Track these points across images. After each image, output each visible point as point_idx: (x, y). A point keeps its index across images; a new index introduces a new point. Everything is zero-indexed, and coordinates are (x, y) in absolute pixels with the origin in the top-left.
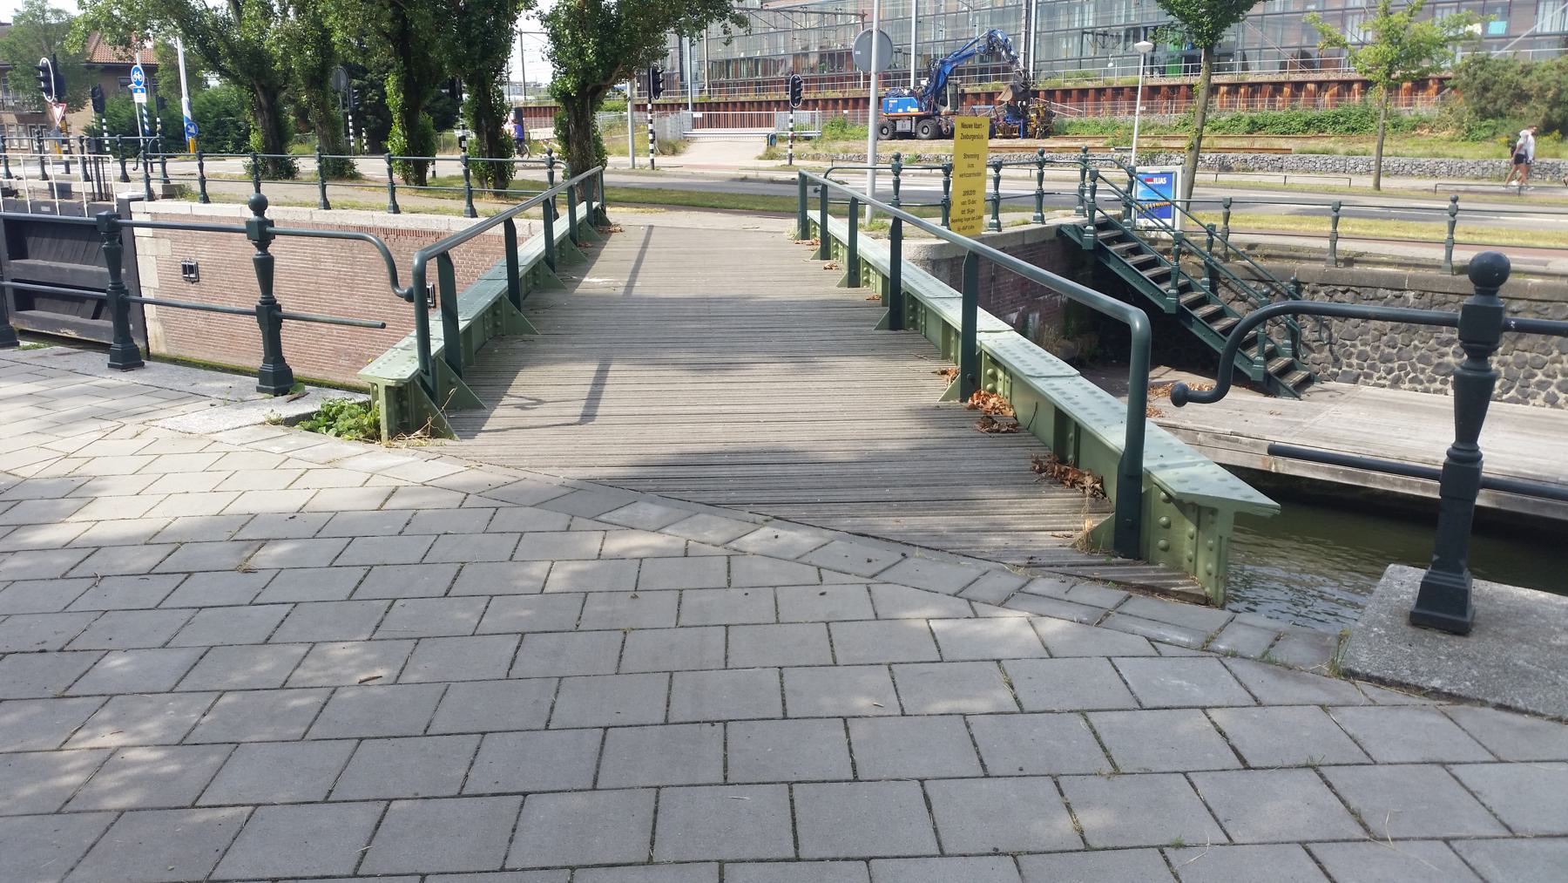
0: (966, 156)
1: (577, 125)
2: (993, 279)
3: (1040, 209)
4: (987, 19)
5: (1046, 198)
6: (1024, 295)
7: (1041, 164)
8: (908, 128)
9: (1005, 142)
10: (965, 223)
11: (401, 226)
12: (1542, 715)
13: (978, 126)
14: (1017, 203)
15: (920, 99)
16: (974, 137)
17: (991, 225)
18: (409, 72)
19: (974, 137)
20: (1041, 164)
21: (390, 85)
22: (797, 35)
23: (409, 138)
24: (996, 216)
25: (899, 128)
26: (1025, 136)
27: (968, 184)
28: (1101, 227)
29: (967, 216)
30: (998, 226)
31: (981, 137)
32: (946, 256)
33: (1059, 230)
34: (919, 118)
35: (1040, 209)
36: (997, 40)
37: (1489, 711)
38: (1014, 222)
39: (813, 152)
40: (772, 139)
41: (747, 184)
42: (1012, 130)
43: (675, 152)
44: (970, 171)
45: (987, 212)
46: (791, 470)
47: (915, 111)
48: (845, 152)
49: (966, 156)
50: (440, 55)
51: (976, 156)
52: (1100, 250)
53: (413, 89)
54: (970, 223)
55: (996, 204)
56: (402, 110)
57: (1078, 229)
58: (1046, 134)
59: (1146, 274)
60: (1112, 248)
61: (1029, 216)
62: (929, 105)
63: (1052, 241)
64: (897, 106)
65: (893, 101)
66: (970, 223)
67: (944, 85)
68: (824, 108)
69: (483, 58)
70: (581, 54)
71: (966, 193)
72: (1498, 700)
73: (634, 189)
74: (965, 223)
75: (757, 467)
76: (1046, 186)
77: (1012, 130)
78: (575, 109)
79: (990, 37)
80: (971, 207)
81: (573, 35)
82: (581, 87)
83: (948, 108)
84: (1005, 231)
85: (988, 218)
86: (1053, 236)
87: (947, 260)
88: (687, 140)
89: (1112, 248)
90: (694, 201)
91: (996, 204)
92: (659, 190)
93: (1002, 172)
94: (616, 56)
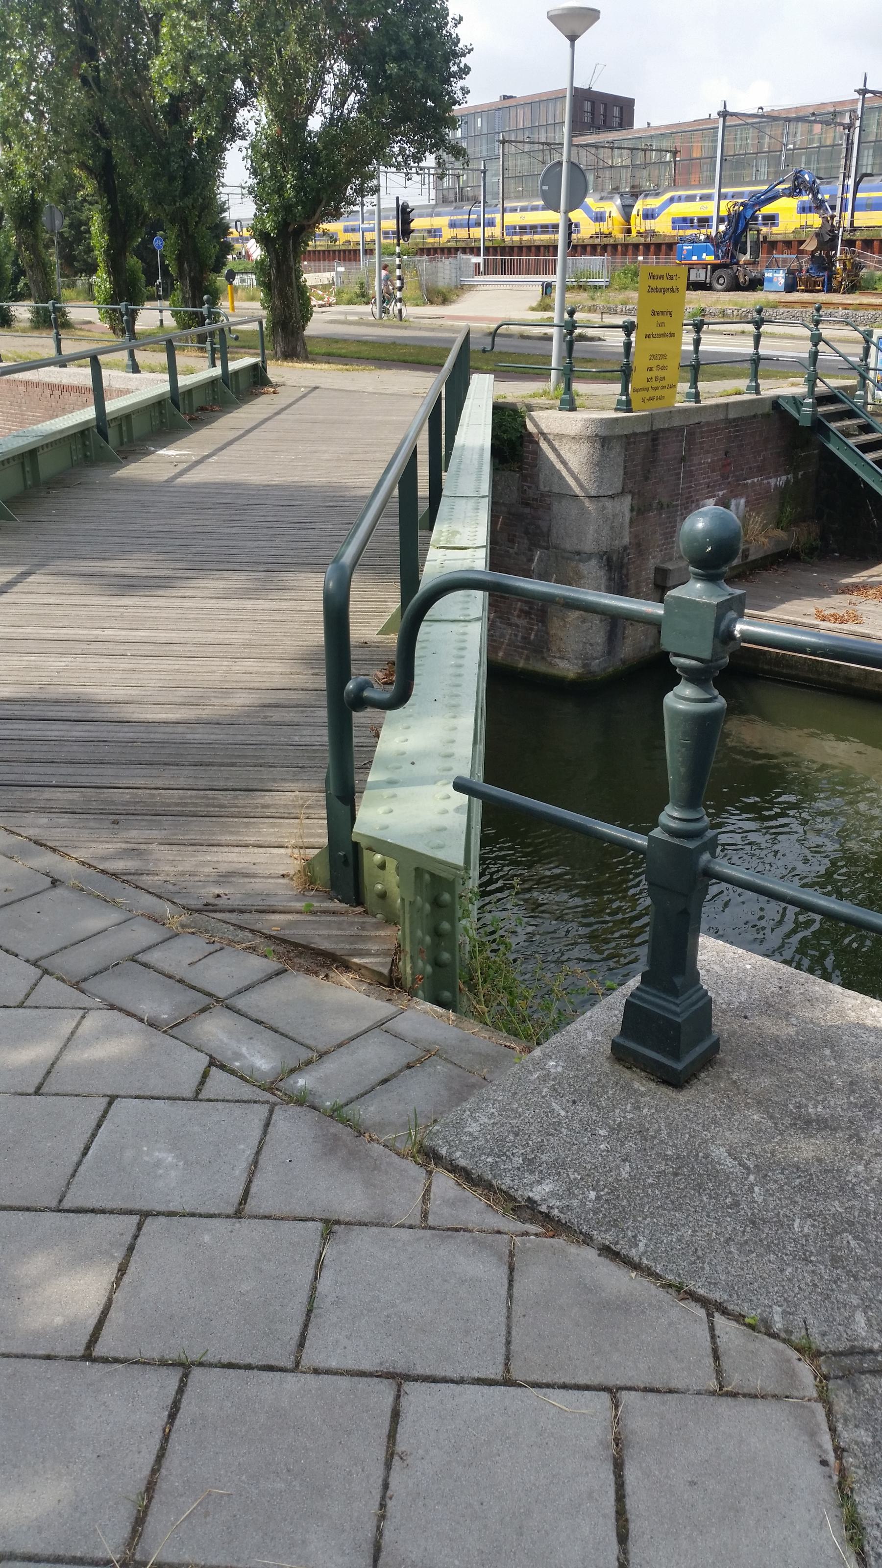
0: (654, 313)
1: (279, 270)
2: (683, 459)
3: (755, 376)
4: (814, 158)
5: (762, 365)
6: (724, 477)
7: (758, 324)
8: (702, 278)
9: (807, 297)
10: (652, 393)
11: (65, 381)
12: (657, 1277)
13: (671, 278)
14: (724, 366)
15: (717, 246)
16: (665, 290)
17: (688, 395)
18: (114, 210)
19: (665, 290)
20: (758, 324)
21: (96, 226)
22: (607, 173)
23: (116, 284)
24: (694, 384)
25: (693, 278)
26: (830, 290)
27: (659, 345)
28: (822, 400)
29: (655, 384)
30: (697, 397)
31: (675, 290)
32: (618, 431)
33: (775, 403)
34: (715, 267)
35: (755, 376)
36: (804, 181)
37: (590, 1254)
38: (718, 392)
39: (590, 303)
40: (547, 288)
41: (528, 343)
42: (816, 283)
43: (445, 300)
44: (661, 330)
45: (683, 380)
46: (55, 731)
47: (710, 258)
48: (625, 303)
49: (654, 313)
50: (139, 192)
51: (669, 313)
52: (819, 426)
53: (119, 227)
54: (659, 393)
55: (696, 369)
56: (107, 252)
57: (796, 401)
58: (853, 288)
59: (869, 457)
60: (833, 426)
61: (743, 384)
62: (727, 253)
63: (766, 416)
64: (691, 253)
65: (687, 247)
66: (659, 393)
67: (745, 230)
68: (614, 254)
69: (185, 193)
70: (280, 190)
71: (653, 357)
72: (607, 1238)
73: (365, 343)
74: (652, 393)
75: (39, 725)
76: (762, 351)
77: (816, 283)
78: (275, 250)
79: (796, 178)
80: (661, 373)
81: (273, 168)
82: (283, 227)
83: (747, 257)
84: (703, 403)
85: (684, 387)
86: (767, 409)
87: (619, 437)
88: (461, 288)
89: (833, 426)
90: (422, 358)
91: (696, 369)
92: (394, 344)
93: (765, 328)
94: (318, 191)
